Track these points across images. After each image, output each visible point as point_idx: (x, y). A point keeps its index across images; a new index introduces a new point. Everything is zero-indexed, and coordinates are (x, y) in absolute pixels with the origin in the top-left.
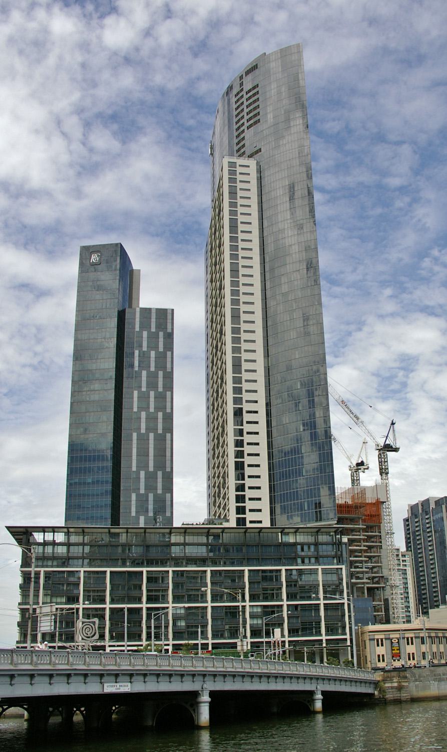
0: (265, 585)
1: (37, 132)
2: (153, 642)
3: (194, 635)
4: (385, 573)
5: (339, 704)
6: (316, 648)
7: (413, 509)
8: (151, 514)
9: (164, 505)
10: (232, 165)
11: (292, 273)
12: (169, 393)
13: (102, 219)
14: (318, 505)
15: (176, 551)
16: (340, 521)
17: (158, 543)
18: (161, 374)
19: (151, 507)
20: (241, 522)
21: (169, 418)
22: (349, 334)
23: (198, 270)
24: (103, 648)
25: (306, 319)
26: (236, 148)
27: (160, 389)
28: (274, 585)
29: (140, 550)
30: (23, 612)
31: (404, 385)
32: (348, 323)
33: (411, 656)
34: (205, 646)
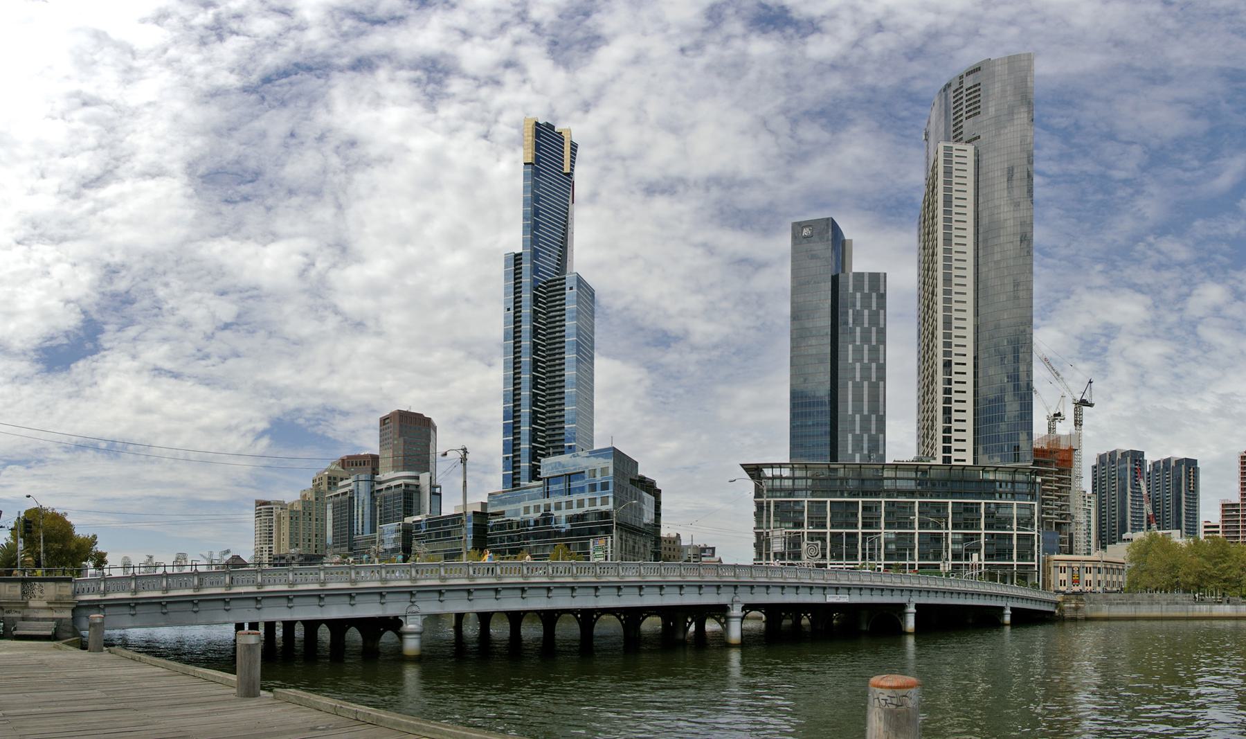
0: (966, 515)
1: (743, 133)
2: (868, 562)
3: (903, 557)
4: (1072, 511)
5: (1024, 618)
6: (1008, 571)
7: (1101, 458)
8: (866, 452)
9: (877, 444)
10: (948, 153)
11: (1007, 242)
12: (881, 347)
13: (814, 197)
14: (1017, 448)
15: (888, 484)
16: (1036, 463)
17: (871, 479)
18: (874, 329)
19: (865, 446)
20: (947, 460)
21: (882, 369)
22: (1057, 300)
23: (911, 238)
24: (825, 565)
25: (1016, 285)
26: (952, 135)
27: (874, 343)
28: (974, 516)
29: (856, 483)
30: (758, 535)
31: (1105, 349)
32: (1057, 291)
33: (1088, 583)
34: (912, 566)
